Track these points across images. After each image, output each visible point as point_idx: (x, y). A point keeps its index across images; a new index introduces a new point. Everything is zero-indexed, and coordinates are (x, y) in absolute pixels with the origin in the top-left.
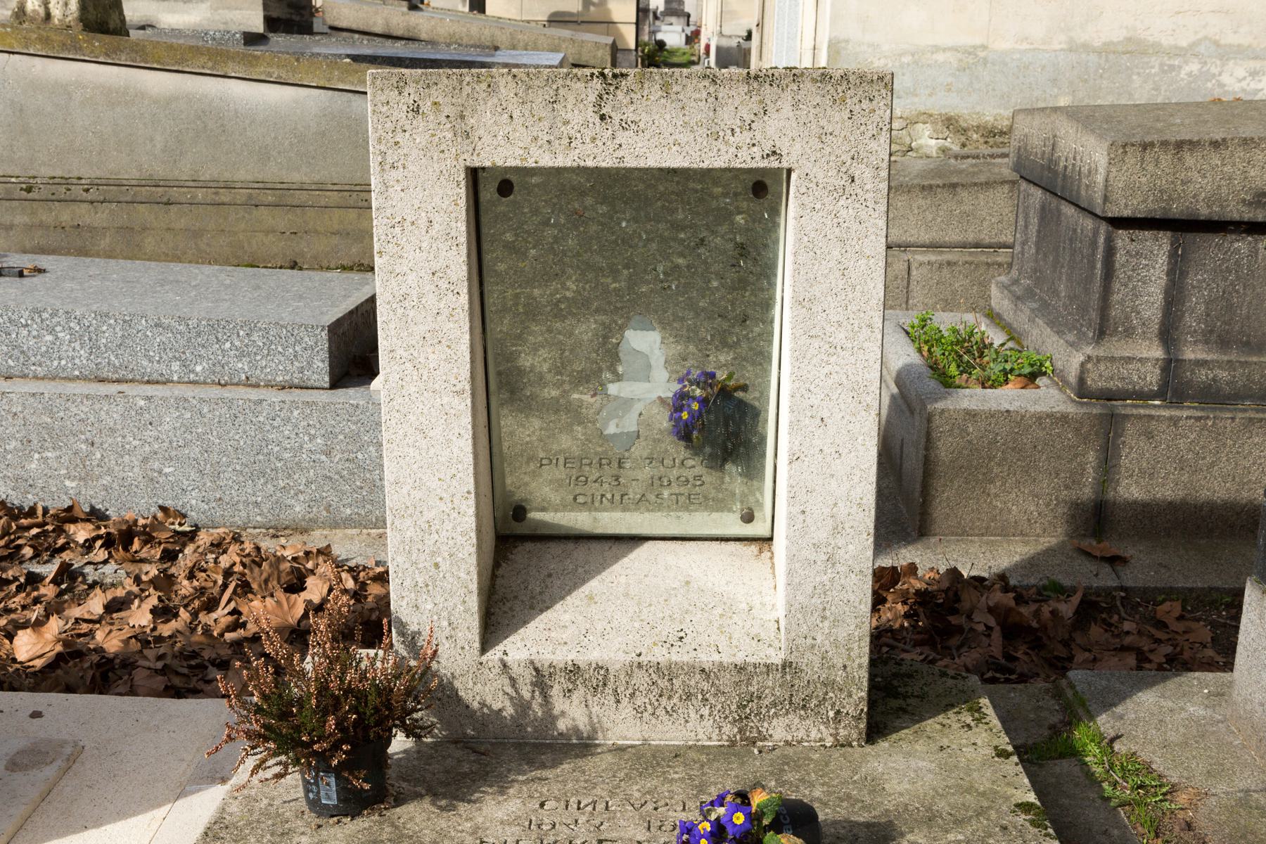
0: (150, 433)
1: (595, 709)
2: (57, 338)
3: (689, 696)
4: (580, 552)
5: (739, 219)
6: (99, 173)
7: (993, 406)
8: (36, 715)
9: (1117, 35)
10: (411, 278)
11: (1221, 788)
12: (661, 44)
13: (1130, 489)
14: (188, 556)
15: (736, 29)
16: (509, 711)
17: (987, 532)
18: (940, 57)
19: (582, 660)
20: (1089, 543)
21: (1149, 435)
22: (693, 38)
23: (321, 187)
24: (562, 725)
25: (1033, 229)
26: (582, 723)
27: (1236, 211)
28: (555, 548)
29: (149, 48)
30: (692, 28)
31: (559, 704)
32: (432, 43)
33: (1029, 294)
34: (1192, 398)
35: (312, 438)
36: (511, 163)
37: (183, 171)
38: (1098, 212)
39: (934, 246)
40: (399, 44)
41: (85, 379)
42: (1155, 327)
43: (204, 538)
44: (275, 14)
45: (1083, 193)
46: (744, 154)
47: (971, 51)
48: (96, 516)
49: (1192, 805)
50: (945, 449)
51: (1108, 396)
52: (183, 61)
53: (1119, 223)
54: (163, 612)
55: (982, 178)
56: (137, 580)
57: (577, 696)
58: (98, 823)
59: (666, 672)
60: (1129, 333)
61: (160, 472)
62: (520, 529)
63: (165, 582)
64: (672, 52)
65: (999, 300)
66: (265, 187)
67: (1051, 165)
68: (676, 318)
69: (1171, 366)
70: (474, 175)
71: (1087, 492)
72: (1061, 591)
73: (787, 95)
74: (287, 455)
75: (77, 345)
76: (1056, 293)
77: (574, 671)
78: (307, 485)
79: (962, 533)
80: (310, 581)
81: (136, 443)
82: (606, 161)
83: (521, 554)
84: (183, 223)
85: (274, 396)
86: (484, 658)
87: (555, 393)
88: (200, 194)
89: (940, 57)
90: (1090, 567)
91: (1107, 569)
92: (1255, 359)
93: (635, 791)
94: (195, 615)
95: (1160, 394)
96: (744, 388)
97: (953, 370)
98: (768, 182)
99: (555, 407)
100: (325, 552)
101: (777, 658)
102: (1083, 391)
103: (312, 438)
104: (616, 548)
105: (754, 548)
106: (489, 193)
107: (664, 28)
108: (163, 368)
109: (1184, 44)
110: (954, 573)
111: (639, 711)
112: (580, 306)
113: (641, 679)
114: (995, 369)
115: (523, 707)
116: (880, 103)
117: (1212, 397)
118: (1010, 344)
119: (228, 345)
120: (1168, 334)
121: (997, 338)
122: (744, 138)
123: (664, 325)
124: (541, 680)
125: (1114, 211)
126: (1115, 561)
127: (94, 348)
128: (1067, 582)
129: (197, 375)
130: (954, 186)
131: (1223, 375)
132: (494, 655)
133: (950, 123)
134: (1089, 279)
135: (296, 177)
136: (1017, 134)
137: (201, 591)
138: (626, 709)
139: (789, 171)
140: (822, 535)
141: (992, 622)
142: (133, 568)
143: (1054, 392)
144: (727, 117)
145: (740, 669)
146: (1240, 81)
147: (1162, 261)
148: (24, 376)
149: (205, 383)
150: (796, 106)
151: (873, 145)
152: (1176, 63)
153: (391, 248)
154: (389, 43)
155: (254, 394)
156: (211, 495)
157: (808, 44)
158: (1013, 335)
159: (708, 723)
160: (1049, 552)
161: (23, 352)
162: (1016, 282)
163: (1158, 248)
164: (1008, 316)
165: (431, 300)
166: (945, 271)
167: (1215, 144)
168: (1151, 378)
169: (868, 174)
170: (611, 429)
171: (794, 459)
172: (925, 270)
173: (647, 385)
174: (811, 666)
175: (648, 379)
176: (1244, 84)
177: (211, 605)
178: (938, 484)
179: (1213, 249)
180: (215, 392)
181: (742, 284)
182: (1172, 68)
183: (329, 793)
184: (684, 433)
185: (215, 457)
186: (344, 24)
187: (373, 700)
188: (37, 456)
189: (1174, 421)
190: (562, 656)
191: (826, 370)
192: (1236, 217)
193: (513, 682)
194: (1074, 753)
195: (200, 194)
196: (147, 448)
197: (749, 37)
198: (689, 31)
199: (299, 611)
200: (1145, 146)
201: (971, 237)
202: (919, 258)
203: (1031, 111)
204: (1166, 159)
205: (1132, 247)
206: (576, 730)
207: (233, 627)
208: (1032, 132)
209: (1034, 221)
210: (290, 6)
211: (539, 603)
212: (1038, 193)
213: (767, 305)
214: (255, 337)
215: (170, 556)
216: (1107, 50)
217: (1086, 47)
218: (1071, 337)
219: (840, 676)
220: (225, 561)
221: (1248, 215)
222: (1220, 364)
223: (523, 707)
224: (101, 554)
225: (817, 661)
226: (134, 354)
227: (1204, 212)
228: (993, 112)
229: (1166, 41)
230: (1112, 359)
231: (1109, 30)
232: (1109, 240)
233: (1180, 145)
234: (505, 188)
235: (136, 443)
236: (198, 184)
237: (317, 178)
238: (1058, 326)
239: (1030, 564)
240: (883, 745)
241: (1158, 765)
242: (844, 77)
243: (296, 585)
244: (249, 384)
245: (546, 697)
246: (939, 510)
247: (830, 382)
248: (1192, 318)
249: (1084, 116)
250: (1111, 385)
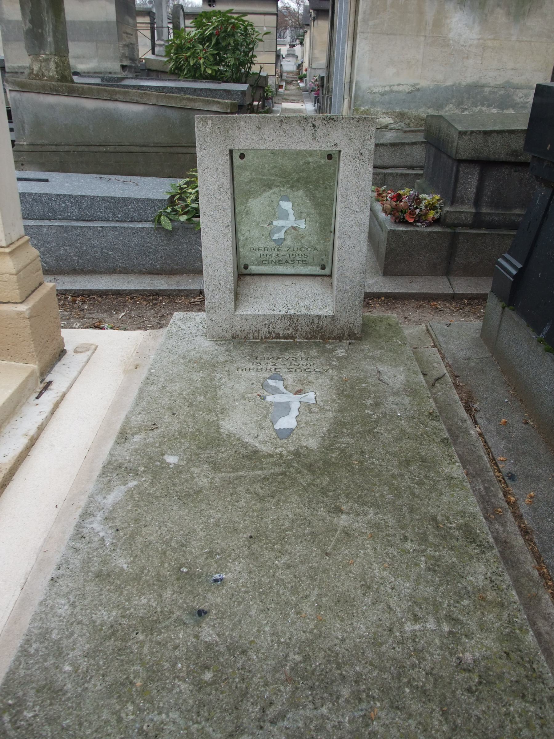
2: (66, 205)
38: (454, 157)
45: (449, 150)
53: (461, 161)
60: (463, 203)
61: (107, 254)
62: (246, 272)
70: (231, 151)
74: (153, 247)
75: (74, 208)
78: (162, 257)
81: (98, 243)
86: (236, 313)
92: (508, 213)
103: (163, 241)
106: (237, 161)
117: (491, 226)
119: (130, 207)
120: (477, 203)
125: (459, 157)
127: (80, 208)
129: (119, 218)
139: (340, 151)
146: (520, 98)
148: (55, 219)
149: (122, 221)
151: (369, 143)
152: (496, 90)
161: (54, 210)
165: (217, 195)
173: (287, 221)
175: (288, 219)
176: (522, 100)
185: (127, 248)
186: (154, 68)
188: (62, 248)
191: (351, 219)
192: (504, 160)
196: (102, 245)
209: (432, 159)
214: (140, 204)
226: (95, 211)
230: (456, 212)
235: (98, 243)
247: (352, 223)
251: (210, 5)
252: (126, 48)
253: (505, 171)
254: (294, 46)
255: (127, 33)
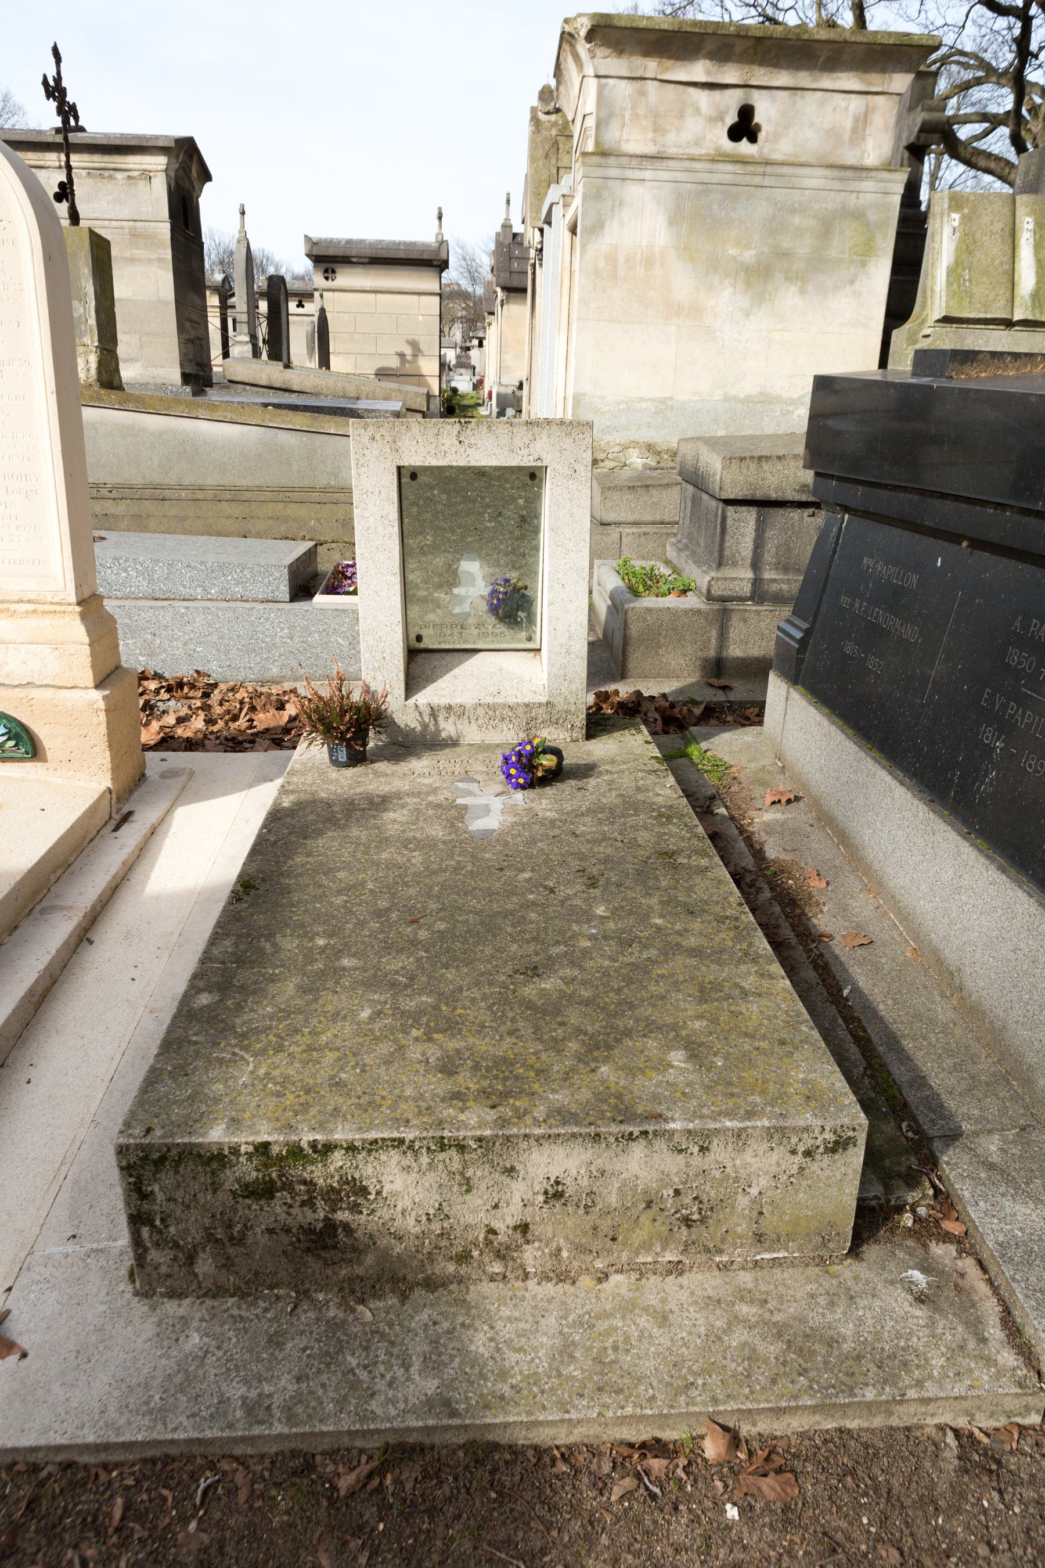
0: (188, 628)
1: (459, 727)
3: (503, 719)
4: (449, 657)
5: (521, 502)
6: (117, 481)
7: (661, 606)
8: (163, 760)
9: (754, 391)
10: (371, 519)
11: (753, 765)
12: (455, 390)
13: (735, 651)
14: (216, 695)
15: (511, 380)
16: (419, 728)
17: (658, 676)
18: (644, 405)
19: (453, 703)
20: (715, 681)
21: (745, 621)
22: (478, 385)
23: (260, 489)
24: (444, 735)
25: (689, 509)
26: (453, 734)
27: (791, 496)
28: (437, 656)
29: (147, 400)
30: (477, 377)
31: (442, 724)
32: (317, 395)
33: (686, 547)
34: (768, 600)
35: (282, 629)
36: (418, 464)
37: (172, 479)
39: (635, 523)
40: (294, 395)
41: (146, 598)
42: (749, 561)
43: (223, 687)
44: (188, 371)
46: (525, 459)
47: (663, 401)
48: (157, 676)
49: (739, 771)
50: (634, 630)
51: (723, 599)
52: (169, 408)
53: (728, 502)
54: (210, 721)
55: (665, 482)
56: (190, 707)
57: (450, 720)
58: (214, 797)
59: (492, 707)
60: (735, 564)
63: (206, 708)
64: (463, 397)
65: (671, 553)
66: (225, 489)
67: (696, 471)
68: (488, 555)
69: (757, 582)
70: (399, 468)
71: (712, 653)
72: (695, 703)
73: (545, 431)
76: (698, 545)
77: (449, 708)
78: (280, 655)
79: (645, 676)
80: (287, 706)
82: (462, 463)
83: (420, 658)
84: (173, 512)
85: (261, 606)
87: (425, 593)
88: (184, 494)
89: (644, 405)
90: (713, 691)
91: (721, 692)
93: (480, 757)
94: (227, 723)
95: (751, 598)
96: (526, 588)
97: (641, 589)
98: (538, 474)
99: (425, 600)
100: (294, 691)
101: (544, 700)
102: (710, 597)
103: (282, 629)
104: (466, 655)
105: (532, 654)
106: (406, 480)
107: (457, 377)
108: (192, 592)
109: (795, 396)
110: (638, 693)
111: (480, 727)
112: (434, 549)
113: (480, 711)
114: (665, 588)
115: (425, 726)
116: (587, 435)
118: (674, 576)
120: (756, 565)
121: (665, 570)
122: (525, 452)
123: (481, 558)
124: (434, 713)
126: (725, 688)
127: (151, 581)
128: (698, 699)
130: (648, 486)
131: (785, 587)
132: (411, 701)
133: (650, 448)
134: (715, 534)
135: (244, 483)
136: (680, 454)
137: (228, 712)
138: (474, 726)
140: (564, 640)
141: (657, 716)
142: (188, 702)
143: (695, 599)
144: (518, 442)
145: (527, 705)
147: (752, 524)
150: (549, 436)
153: (362, 505)
154: (287, 394)
155: (247, 605)
156: (224, 664)
157: (561, 395)
158: (676, 570)
159: (512, 732)
160: (691, 685)
162: (680, 541)
163: (749, 517)
164: (675, 561)
166: (643, 538)
167: (779, 458)
168: (747, 589)
169: (582, 468)
170: (457, 610)
171: (551, 604)
172: (630, 537)
174: (560, 704)
177: (235, 718)
178: (630, 649)
179: (781, 517)
180: (224, 604)
181: (523, 537)
182: (788, 412)
183: (343, 756)
184: (494, 610)
185: (226, 641)
187: (363, 711)
189: (758, 613)
190: (444, 701)
192: (791, 498)
193: (421, 714)
194: (686, 755)
195: (184, 494)
197: (520, 387)
198: (475, 379)
199: (286, 719)
200: (742, 459)
201: (658, 518)
202: (627, 530)
203: (686, 440)
204: (753, 466)
205: (736, 516)
206: (451, 737)
207: (251, 727)
208: (687, 451)
210: (197, 364)
211: (430, 679)
212: (691, 488)
213: (537, 549)
215: (206, 695)
216: (748, 400)
217: (735, 399)
218: (705, 568)
219: (573, 708)
220: (239, 696)
221: (797, 497)
222: (783, 581)
223: (425, 726)
224: (167, 696)
225: (562, 700)
226: (175, 583)
227: (774, 496)
228: (667, 438)
229: (785, 395)
230: (725, 579)
231: (748, 388)
232: (724, 512)
233: (760, 458)
234: (414, 476)
236: (182, 487)
237: (257, 483)
238: (698, 563)
239: (680, 691)
240: (593, 741)
241: (726, 759)
242: (571, 423)
243: (281, 706)
244: (242, 600)
245: (436, 721)
246: (632, 664)
248: (768, 557)
249: (712, 442)
250: (725, 593)
251: (327, 278)
252: (191, 346)
253: (795, 514)
254: (468, 349)
255: (191, 321)
